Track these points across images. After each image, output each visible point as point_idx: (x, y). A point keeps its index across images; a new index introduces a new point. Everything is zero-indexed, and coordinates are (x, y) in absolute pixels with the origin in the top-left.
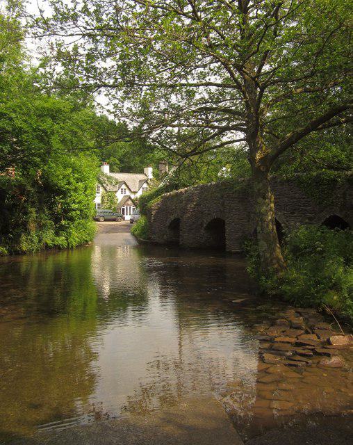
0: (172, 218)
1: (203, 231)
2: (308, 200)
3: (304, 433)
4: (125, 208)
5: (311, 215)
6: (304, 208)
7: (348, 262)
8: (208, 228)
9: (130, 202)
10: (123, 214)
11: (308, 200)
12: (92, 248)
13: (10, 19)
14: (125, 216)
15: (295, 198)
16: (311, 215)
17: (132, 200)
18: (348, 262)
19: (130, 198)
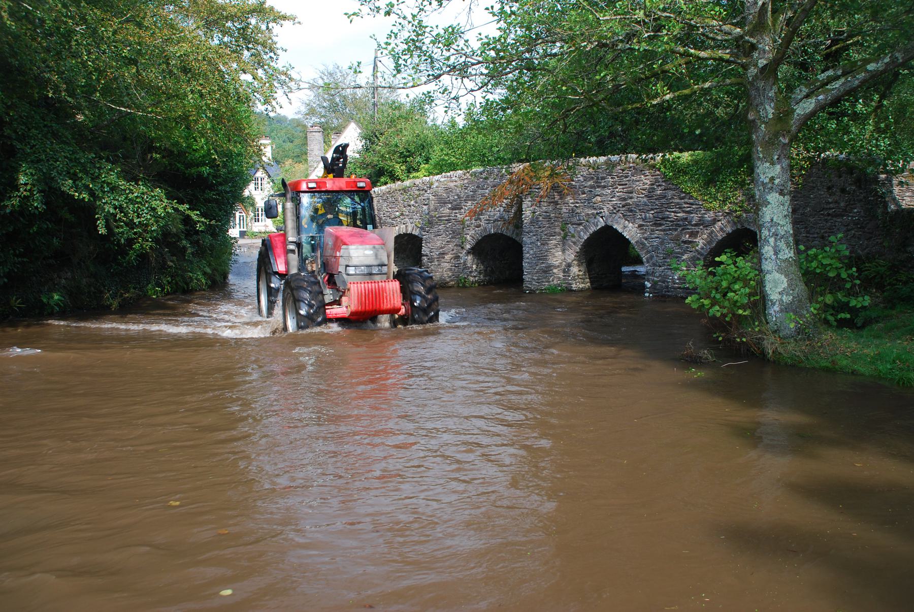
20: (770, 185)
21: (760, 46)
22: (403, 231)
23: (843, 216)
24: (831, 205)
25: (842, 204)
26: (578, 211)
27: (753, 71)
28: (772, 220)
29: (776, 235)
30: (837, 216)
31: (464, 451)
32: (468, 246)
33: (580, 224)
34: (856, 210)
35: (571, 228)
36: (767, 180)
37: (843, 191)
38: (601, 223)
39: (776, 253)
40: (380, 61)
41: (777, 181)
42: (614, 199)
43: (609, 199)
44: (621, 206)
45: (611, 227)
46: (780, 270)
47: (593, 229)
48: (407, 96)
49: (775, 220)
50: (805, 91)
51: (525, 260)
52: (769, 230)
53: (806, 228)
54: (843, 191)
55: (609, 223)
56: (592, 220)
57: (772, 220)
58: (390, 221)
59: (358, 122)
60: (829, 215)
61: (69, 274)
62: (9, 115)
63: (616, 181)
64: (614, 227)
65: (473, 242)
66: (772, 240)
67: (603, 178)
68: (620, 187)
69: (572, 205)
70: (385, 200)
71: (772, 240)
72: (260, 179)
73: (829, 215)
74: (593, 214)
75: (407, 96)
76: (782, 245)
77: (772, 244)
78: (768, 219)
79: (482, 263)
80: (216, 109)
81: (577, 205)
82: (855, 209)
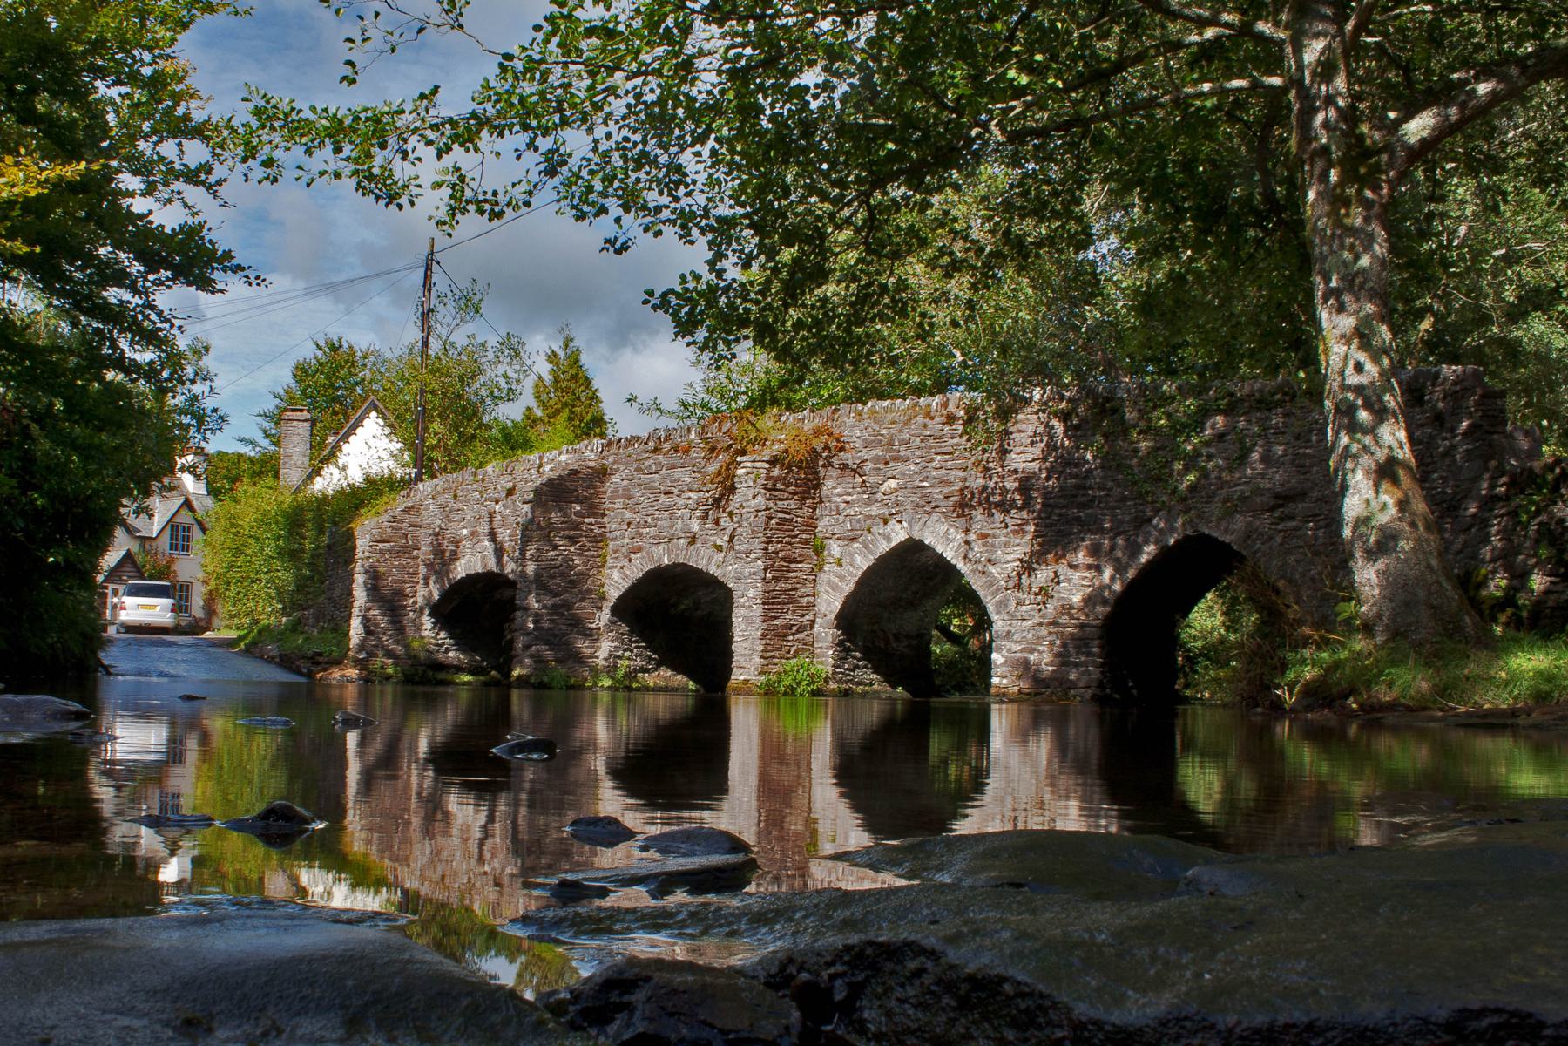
31: (515, 822)
34: (1436, 475)
40: (438, 263)
42: (925, 484)
43: (917, 483)
44: (941, 497)
45: (920, 543)
47: (884, 547)
48: (473, 179)
59: (382, 414)
62: (1100, 826)
63: (931, 447)
64: (927, 542)
68: (939, 457)
69: (839, 500)
72: (181, 529)
75: (473, 179)
79: (964, 586)
80: (1054, 1026)
81: (849, 498)
82: (1434, 472)
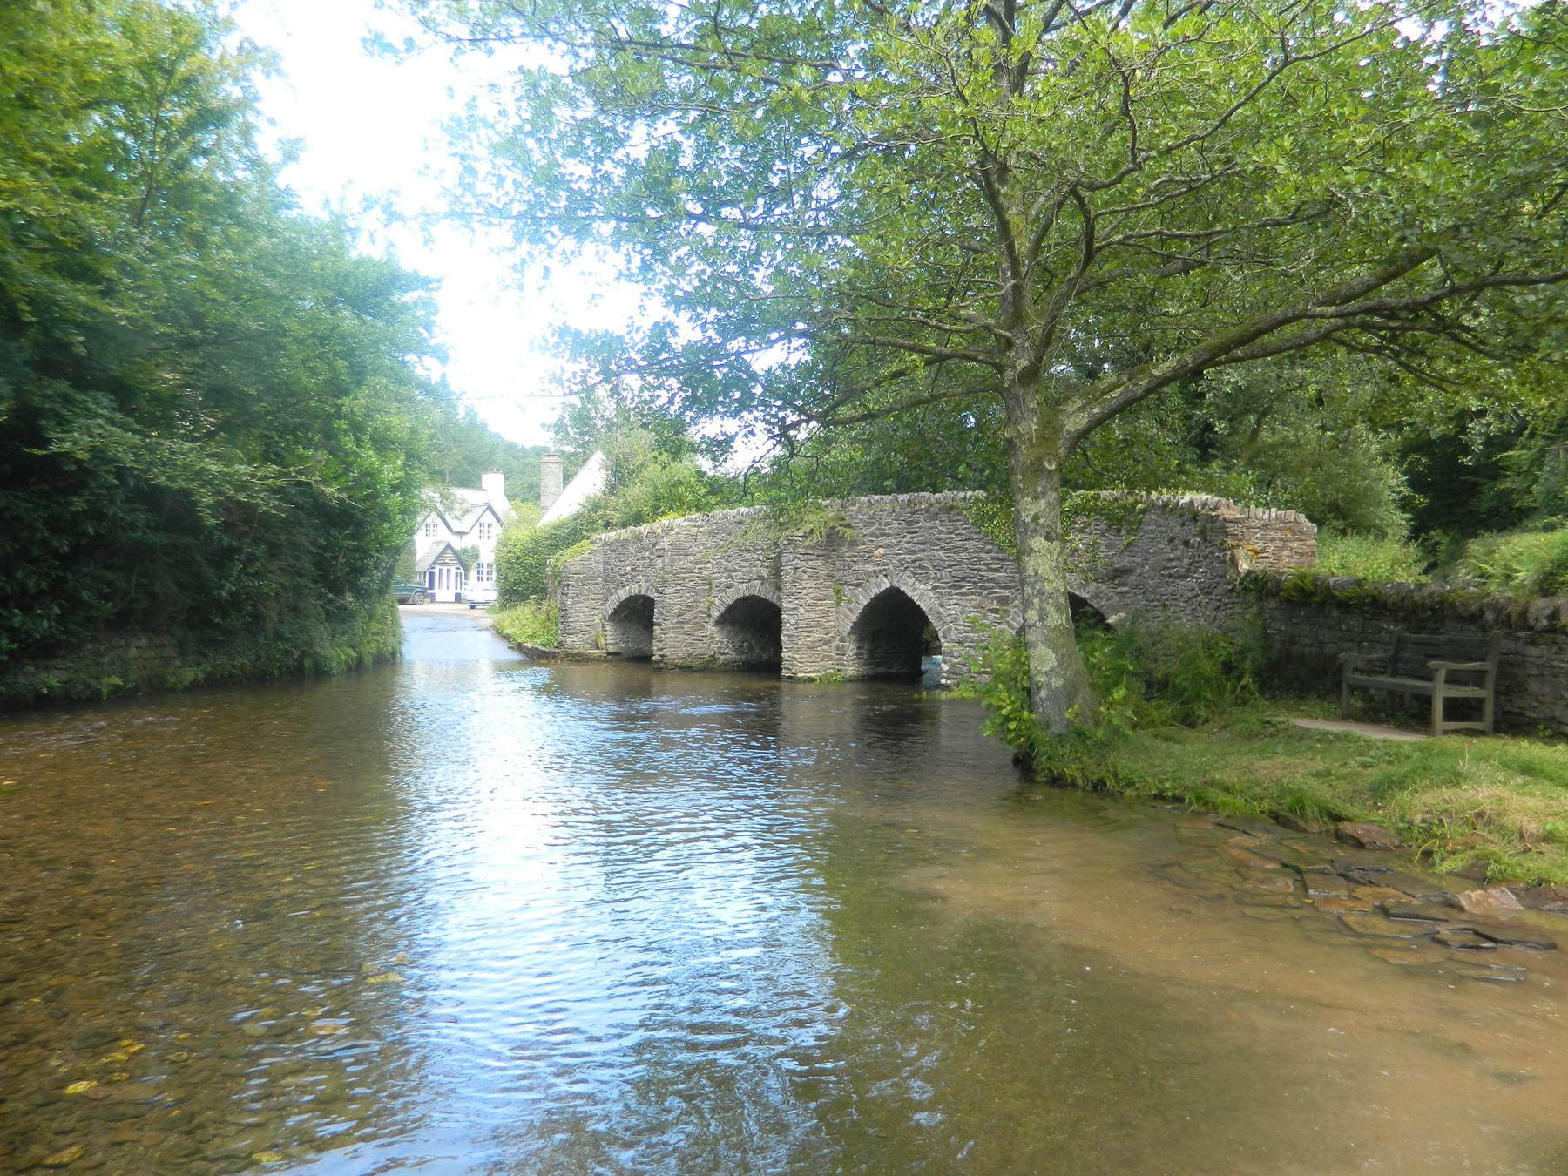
0: (623, 594)
1: (711, 628)
2: (1000, 556)
3: (1219, 199)
4: (436, 571)
5: (1006, 592)
6: (991, 575)
7: (540, 1173)
8: (722, 621)
9: (449, 557)
10: (431, 586)
11: (1000, 556)
12: (1417, 731)
13: (317, 264)
14: (436, 591)
15: (965, 550)
16: (1006, 592)
17: (454, 552)
18: (540, 1173)
19: (449, 546)
20: (1032, 526)
21: (1018, 342)
22: (635, 591)
23: (1186, 577)
24: (1174, 564)
25: (1186, 561)
26: (856, 567)
27: (1009, 374)
28: (1036, 574)
29: (1041, 593)
30: (1180, 577)
32: (716, 614)
33: (858, 585)
35: (847, 590)
36: (1029, 520)
37: (1186, 543)
38: (885, 584)
39: (1042, 619)
41: (1042, 521)
46: (1048, 642)
47: (876, 591)
49: (1040, 572)
50: (1079, 403)
51: (784, 633)
52: (1033, 588)
53: (1144, 593)
54: (1186, 543)
55: (896, 584)
56: (873, 580)
57: (1036, 574)
58: (619, 578)
60: (1170, 576)
61: (144, 641)
65: (722, 609)
66: (1036, 601)
67: (888, 524)
70: (613, 551)
71: (1036, 601)
73: (1170, 576)
74: (874, 572)
76: (1051, 609)
77: (1037, 606)
78: (1031, 571)
